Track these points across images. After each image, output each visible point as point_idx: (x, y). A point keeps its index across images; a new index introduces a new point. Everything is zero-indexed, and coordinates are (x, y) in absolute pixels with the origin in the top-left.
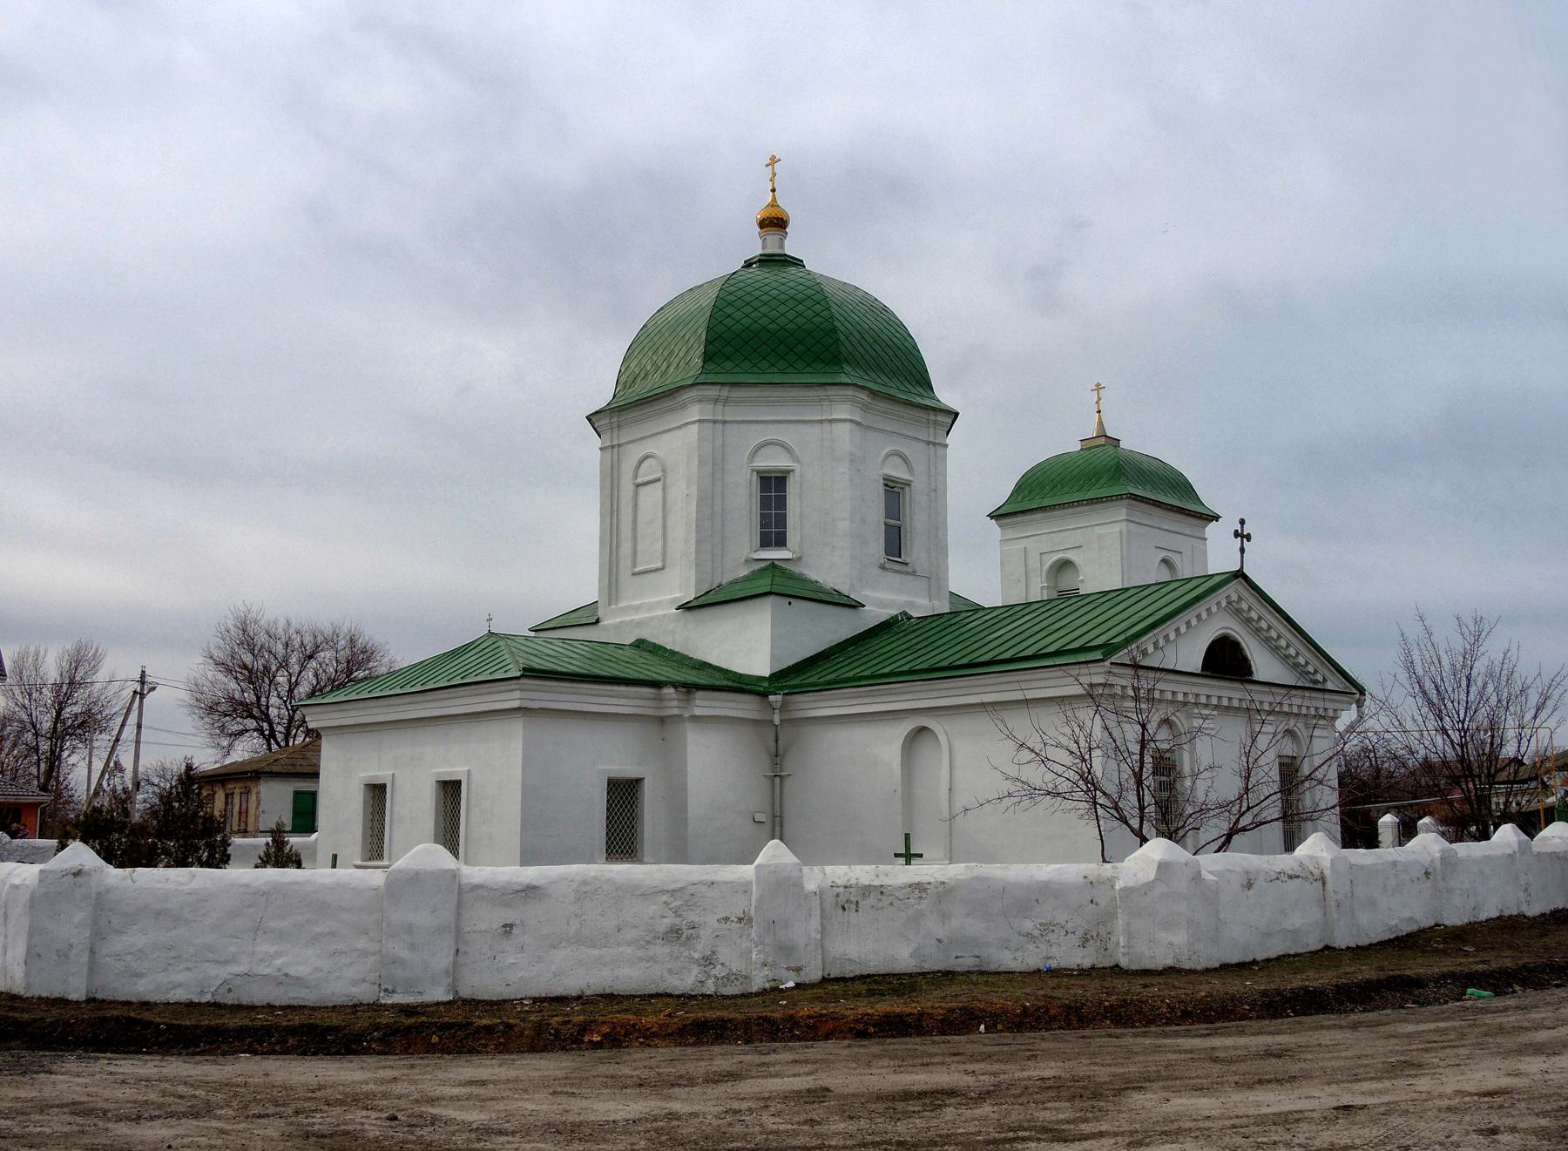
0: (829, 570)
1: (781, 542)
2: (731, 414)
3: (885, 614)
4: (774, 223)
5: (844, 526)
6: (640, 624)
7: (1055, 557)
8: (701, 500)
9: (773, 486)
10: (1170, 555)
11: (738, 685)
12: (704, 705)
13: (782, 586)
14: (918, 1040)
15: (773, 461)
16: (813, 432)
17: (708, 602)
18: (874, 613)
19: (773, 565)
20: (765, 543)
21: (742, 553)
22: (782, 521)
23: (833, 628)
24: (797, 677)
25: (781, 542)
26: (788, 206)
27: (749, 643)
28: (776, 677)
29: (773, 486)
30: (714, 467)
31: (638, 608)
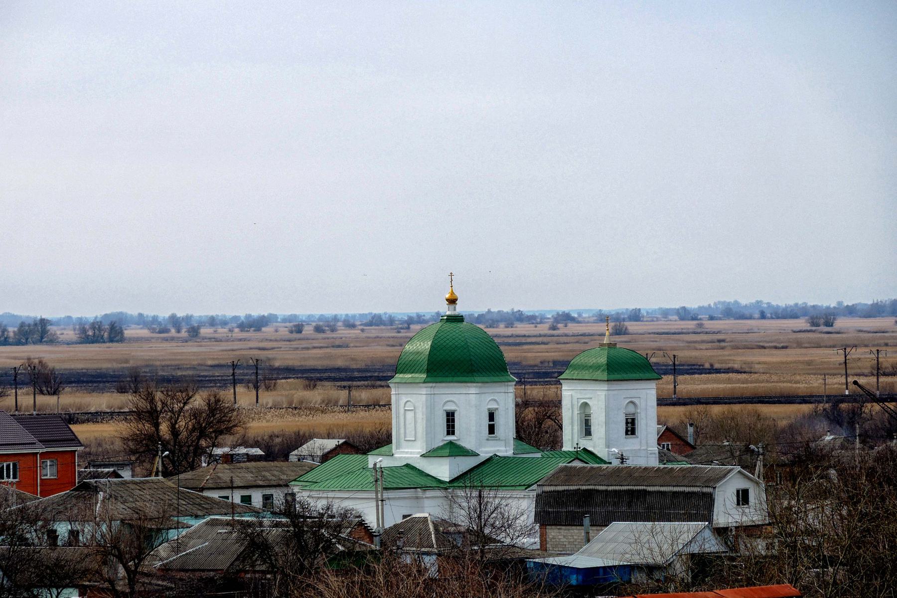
0: (468, 443)
1: (453, 433)
2: (436, 391)
3: (488, 456)
4: (452, 301)
5: (473, 429)
6: (408, 458)
7: (583, 401)
8: (427, 420)
9: (450, 417)
10: (633, 400)
11: (439, 484)
12: (429, 493)
13: (454, 450)
14: (105, 434)
15: (450, 407)
16: (462, 397)
17: (431, 454)
18: (484, 456)
19: (451, 443)
20: (448, 434)
21: (441, 438)
22: (453, 426)
23: (467, 463)
24: (458, 480)
25: (453, 433)
26: (457, 294)
27: (443, 470)
28: (451, 482)
29: (450, 417)
30: (431, 409)
31: (407, 453)
